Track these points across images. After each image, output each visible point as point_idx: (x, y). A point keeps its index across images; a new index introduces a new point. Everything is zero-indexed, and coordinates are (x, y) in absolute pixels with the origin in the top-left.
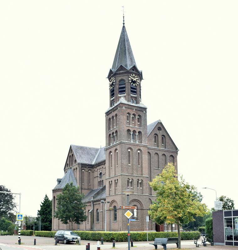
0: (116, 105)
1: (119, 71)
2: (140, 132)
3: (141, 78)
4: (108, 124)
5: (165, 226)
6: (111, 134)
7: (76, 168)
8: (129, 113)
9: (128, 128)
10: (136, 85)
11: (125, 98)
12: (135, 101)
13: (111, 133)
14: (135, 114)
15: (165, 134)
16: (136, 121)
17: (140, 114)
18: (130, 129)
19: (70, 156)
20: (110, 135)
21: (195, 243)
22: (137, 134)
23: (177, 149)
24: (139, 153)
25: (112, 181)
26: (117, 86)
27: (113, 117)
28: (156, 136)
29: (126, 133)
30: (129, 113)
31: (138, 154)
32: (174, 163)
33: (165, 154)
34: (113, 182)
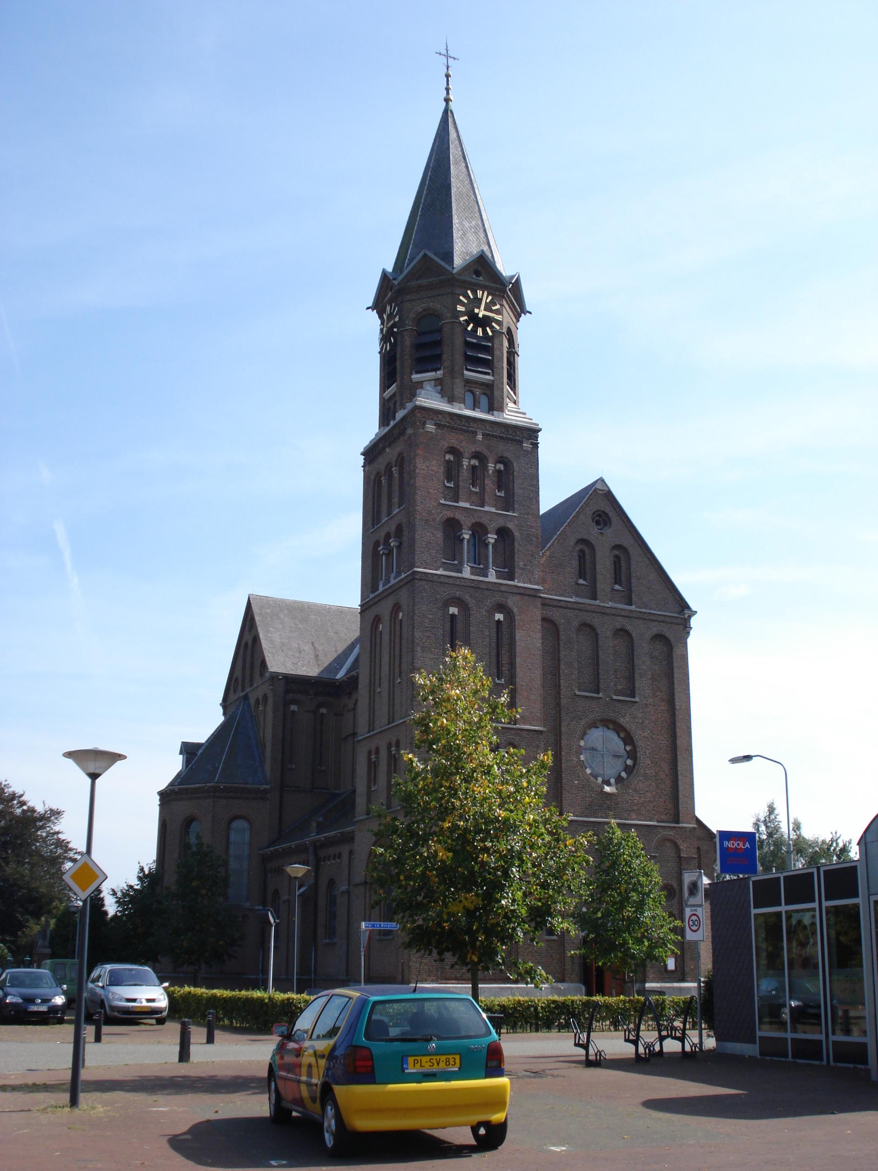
0: (400, 415)
1: (417, 279)
2: (503, 533)
3: (519, 309)
4: (370, 497)
6: (382, 541)
7: (265, 697)
8: (452, 450)
9: (449, 514)
10: (490, 334)
11: (439, 388)
12: (484, 401)
13: (382, 534)
14: (486, 452)
16: (490, 484)
17: (506, 454)
18: (459, 516)
19: (246, 644)
20: (377, 544)
21: (577, 1045)
22: (492, 538)
25: (377, 751)
26: (408, 341)
27: (389, 467)
30: (452, 450)
31: (494, 625)
33: (629, 628)
34: (383, 753)
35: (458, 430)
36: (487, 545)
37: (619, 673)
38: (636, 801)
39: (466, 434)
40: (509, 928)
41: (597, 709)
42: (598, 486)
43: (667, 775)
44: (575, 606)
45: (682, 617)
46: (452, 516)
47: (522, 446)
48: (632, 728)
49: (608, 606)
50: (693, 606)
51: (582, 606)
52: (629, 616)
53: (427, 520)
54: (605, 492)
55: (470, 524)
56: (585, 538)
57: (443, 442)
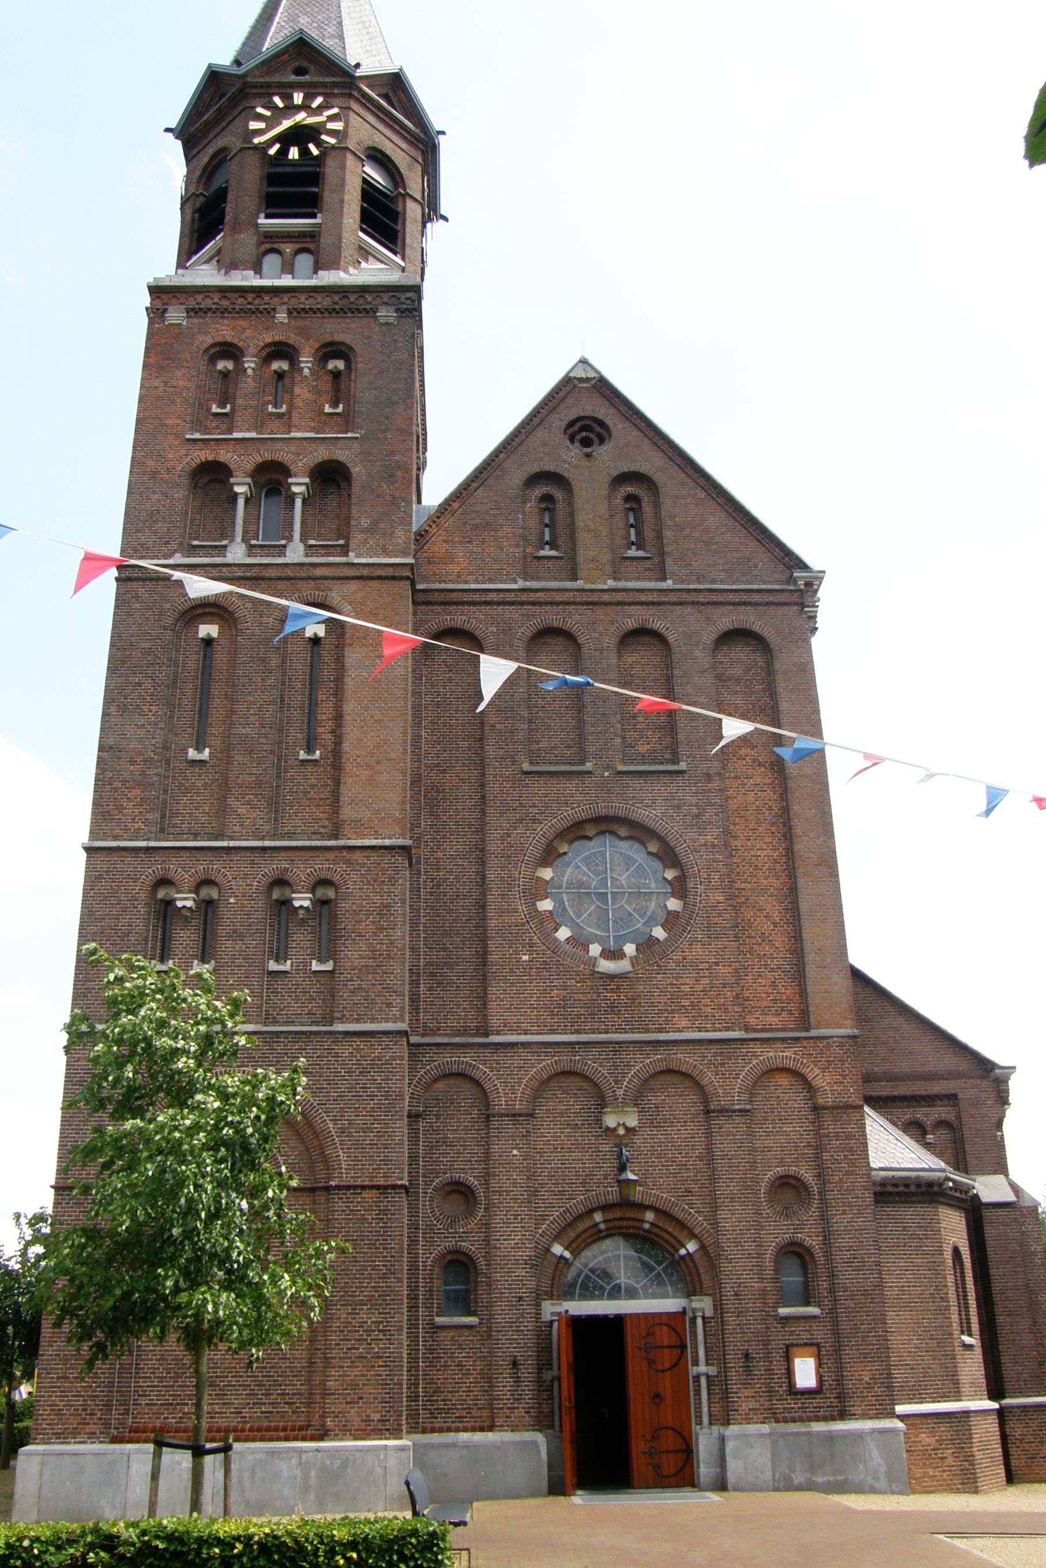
5: (697, 1378)
14: (293, 339)
15: (649, 462)
23: (790, 561)
24: (208, 642)
28: (559, 495)
29: (180, 494)
32: (576, 661)
33: (658, 625)
35: (237, 313)
36: (291, 498)
37: (640, 719)
38: (686, 988)
39: (254, 317)
40: (168, 1207)
41: (579, 797)
42: (579, 373)
43: (775, 925)
44: (524, 597)
45: (792, 587)
46: (210, 458)
47: (376, 318)
48: (672, 828)
49: (605, 587)
50: (814, 562)
51: (541, 595)
52: (658, 602)
53: (155, 473)
54: (593, 382)
55: (250, 467)
56: (547, 468)
57: (201, 338)
